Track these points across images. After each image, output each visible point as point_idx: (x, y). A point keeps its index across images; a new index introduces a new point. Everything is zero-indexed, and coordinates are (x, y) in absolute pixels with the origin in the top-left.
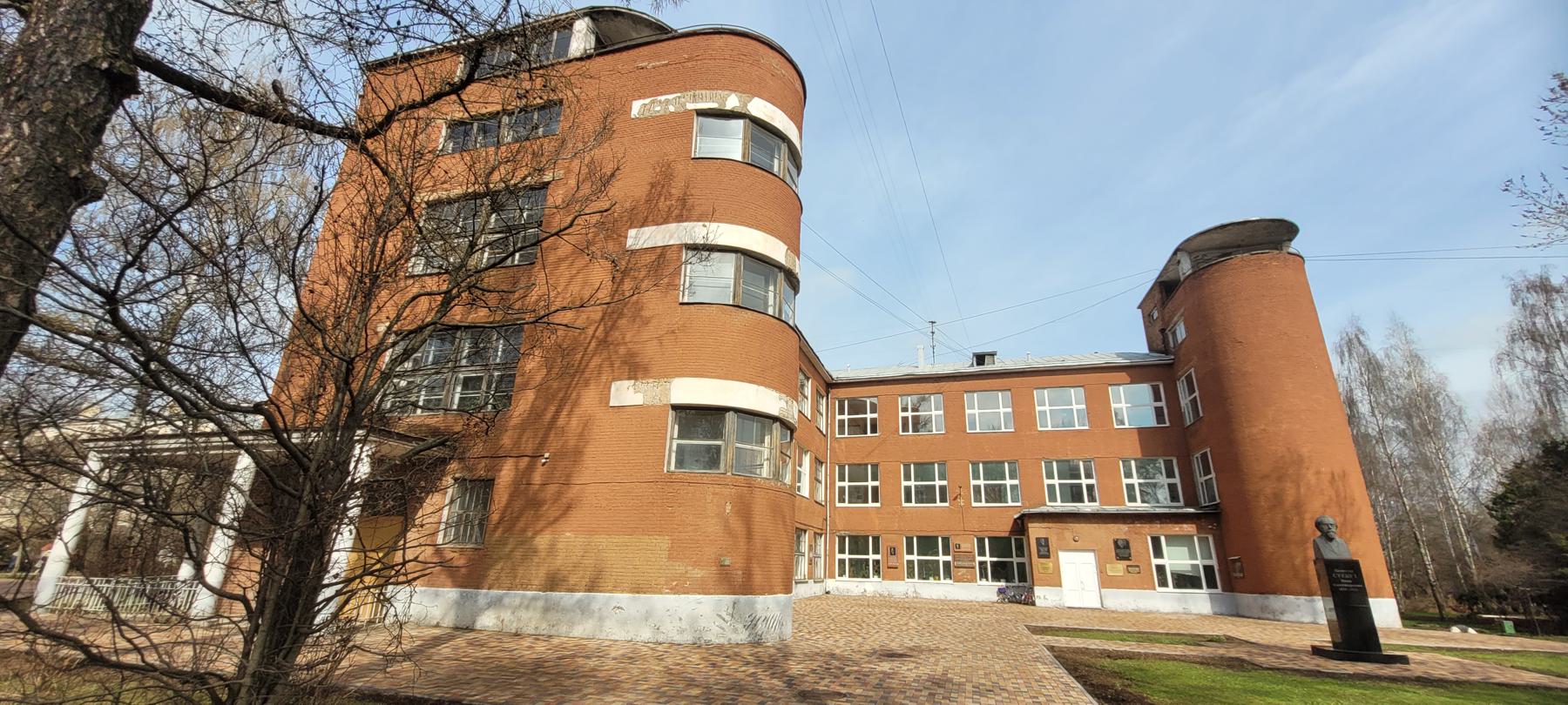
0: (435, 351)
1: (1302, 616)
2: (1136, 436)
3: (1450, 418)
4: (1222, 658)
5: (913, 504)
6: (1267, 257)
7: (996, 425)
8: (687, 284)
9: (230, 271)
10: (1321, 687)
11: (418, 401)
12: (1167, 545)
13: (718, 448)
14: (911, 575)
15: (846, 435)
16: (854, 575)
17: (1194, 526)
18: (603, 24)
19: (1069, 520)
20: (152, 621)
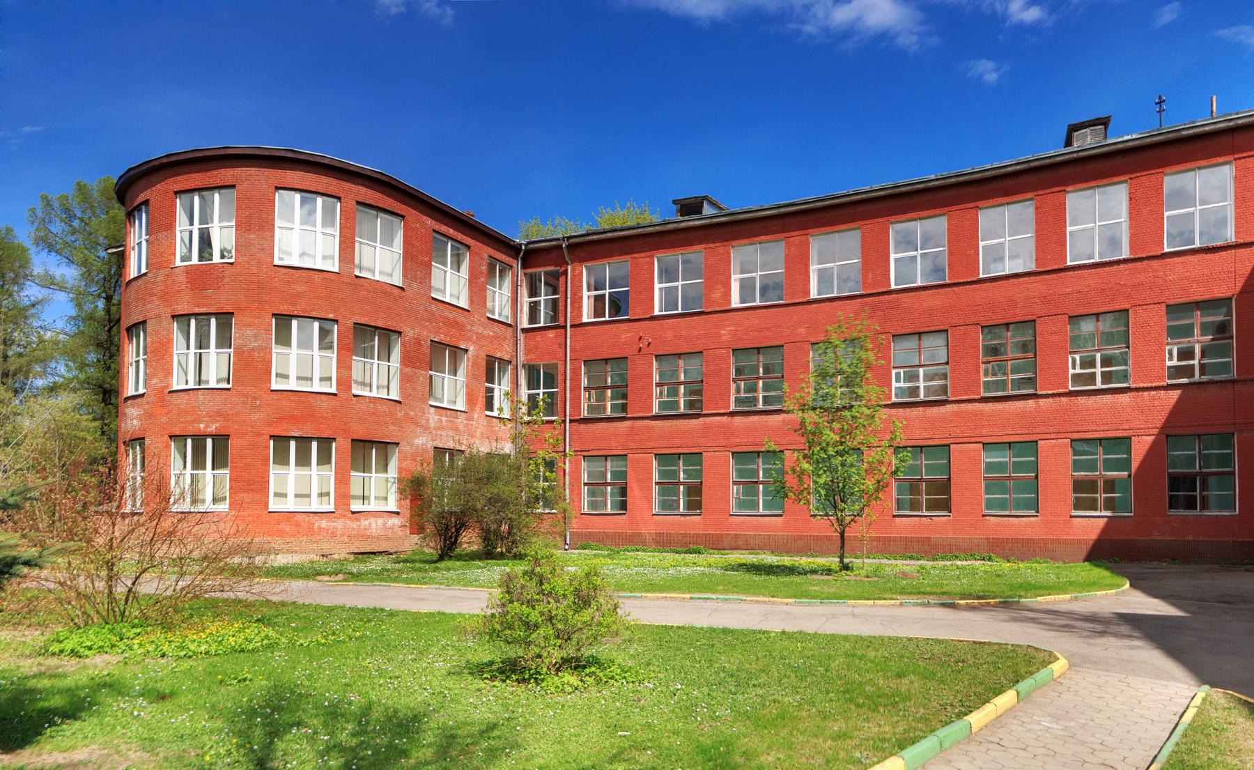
0: (613, 398)
1: (207, 426)
2: (320, 467)
3: (835, 353)
4: (1023, 558)
5: (1130, 368)
6: (324, 376)
7: (575, 335)
8: (856, 611)
9: (844, 740)
10: (462, 604)
11: (914, 391)
12: (274, 463)
13: (1074, 455)
14: (1077, 466)
15: (607, 318)
16: (827, 574)
17: (1039, 7)
18: (665, 364)
19: (360, 181)
20: (255, 519)
